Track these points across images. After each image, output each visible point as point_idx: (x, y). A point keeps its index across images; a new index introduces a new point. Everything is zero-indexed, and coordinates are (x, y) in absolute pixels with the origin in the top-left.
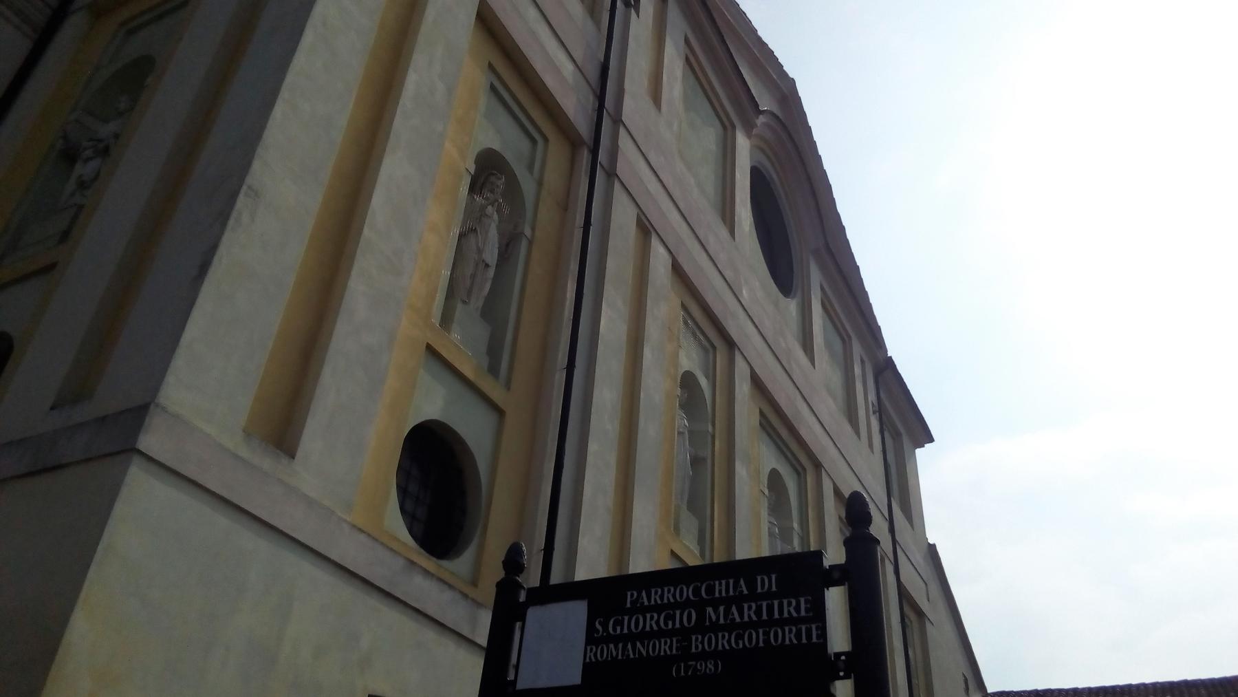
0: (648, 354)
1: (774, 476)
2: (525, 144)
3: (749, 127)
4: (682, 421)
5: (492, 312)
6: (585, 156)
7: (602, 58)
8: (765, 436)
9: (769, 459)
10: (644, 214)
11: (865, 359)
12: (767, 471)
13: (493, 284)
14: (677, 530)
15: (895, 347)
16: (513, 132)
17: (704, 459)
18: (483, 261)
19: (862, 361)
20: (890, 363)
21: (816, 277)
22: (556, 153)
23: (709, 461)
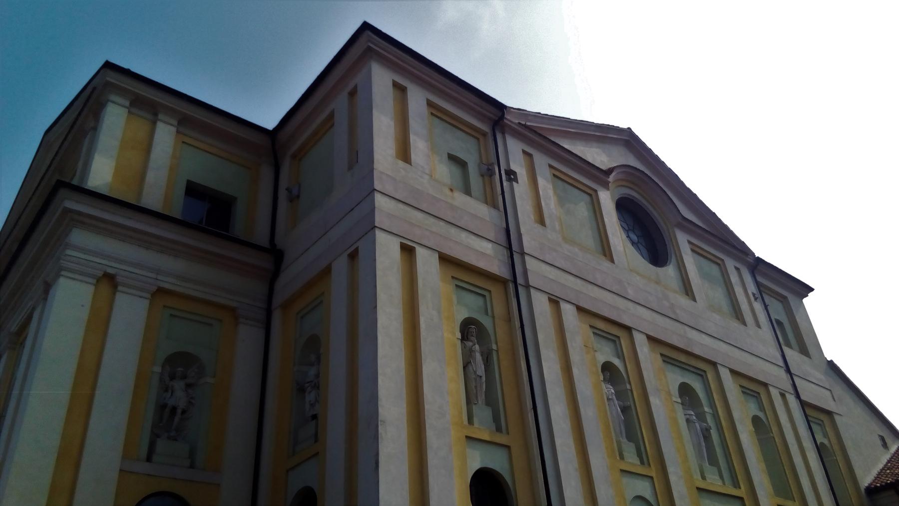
0: (575, 371)
1: (685, 390)
2: (480, 301)
3: (606, 185)
4: (610, 390)
5: (491, 401)
6: (511, 286)
7: (504, 225)
8: (669, 366)
9: (675, 378)
10: (552, 295)
11: (738, 265)
12: (675, 390)
13: (486, 383)
14: (622, 457)
15: (760, 251)
16: (470, 298)
17: (629, 407)
18: (478, 376)
19: (737, 269)
20: (760, 261)
21: (683, 240)
22: (496, 291)
23: (633, 407)
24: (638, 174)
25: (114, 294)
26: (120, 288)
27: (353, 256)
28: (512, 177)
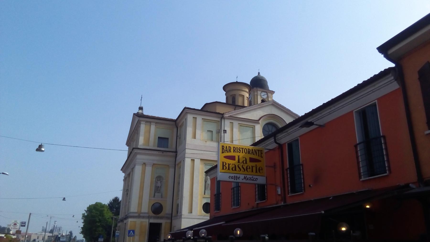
24: (272, 115)
25: (146, 166)
26: (146, 165)
27: (183, 160)
28: (225, 132)
